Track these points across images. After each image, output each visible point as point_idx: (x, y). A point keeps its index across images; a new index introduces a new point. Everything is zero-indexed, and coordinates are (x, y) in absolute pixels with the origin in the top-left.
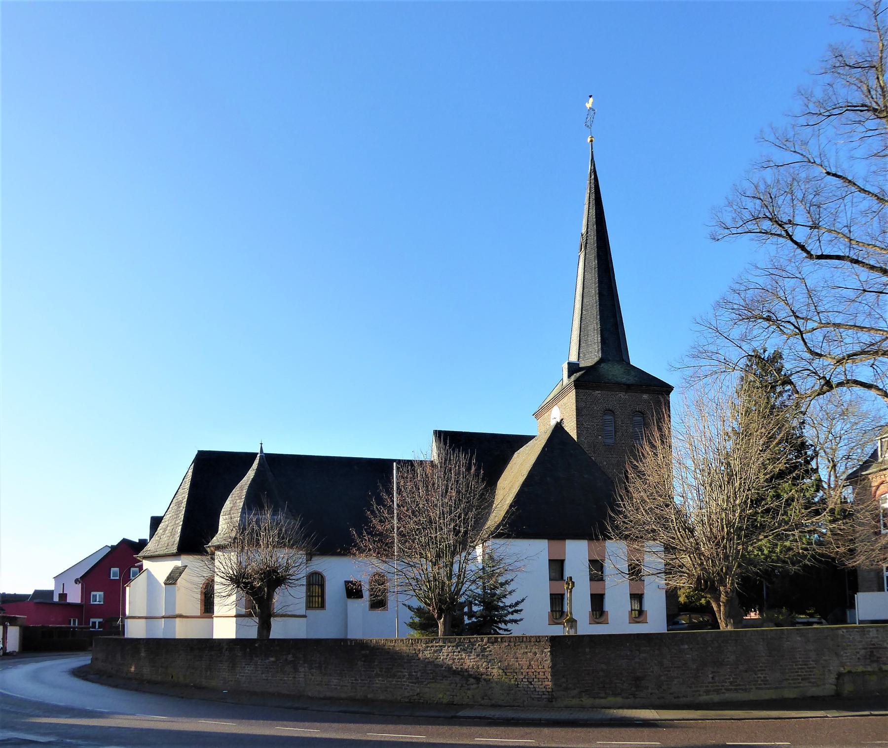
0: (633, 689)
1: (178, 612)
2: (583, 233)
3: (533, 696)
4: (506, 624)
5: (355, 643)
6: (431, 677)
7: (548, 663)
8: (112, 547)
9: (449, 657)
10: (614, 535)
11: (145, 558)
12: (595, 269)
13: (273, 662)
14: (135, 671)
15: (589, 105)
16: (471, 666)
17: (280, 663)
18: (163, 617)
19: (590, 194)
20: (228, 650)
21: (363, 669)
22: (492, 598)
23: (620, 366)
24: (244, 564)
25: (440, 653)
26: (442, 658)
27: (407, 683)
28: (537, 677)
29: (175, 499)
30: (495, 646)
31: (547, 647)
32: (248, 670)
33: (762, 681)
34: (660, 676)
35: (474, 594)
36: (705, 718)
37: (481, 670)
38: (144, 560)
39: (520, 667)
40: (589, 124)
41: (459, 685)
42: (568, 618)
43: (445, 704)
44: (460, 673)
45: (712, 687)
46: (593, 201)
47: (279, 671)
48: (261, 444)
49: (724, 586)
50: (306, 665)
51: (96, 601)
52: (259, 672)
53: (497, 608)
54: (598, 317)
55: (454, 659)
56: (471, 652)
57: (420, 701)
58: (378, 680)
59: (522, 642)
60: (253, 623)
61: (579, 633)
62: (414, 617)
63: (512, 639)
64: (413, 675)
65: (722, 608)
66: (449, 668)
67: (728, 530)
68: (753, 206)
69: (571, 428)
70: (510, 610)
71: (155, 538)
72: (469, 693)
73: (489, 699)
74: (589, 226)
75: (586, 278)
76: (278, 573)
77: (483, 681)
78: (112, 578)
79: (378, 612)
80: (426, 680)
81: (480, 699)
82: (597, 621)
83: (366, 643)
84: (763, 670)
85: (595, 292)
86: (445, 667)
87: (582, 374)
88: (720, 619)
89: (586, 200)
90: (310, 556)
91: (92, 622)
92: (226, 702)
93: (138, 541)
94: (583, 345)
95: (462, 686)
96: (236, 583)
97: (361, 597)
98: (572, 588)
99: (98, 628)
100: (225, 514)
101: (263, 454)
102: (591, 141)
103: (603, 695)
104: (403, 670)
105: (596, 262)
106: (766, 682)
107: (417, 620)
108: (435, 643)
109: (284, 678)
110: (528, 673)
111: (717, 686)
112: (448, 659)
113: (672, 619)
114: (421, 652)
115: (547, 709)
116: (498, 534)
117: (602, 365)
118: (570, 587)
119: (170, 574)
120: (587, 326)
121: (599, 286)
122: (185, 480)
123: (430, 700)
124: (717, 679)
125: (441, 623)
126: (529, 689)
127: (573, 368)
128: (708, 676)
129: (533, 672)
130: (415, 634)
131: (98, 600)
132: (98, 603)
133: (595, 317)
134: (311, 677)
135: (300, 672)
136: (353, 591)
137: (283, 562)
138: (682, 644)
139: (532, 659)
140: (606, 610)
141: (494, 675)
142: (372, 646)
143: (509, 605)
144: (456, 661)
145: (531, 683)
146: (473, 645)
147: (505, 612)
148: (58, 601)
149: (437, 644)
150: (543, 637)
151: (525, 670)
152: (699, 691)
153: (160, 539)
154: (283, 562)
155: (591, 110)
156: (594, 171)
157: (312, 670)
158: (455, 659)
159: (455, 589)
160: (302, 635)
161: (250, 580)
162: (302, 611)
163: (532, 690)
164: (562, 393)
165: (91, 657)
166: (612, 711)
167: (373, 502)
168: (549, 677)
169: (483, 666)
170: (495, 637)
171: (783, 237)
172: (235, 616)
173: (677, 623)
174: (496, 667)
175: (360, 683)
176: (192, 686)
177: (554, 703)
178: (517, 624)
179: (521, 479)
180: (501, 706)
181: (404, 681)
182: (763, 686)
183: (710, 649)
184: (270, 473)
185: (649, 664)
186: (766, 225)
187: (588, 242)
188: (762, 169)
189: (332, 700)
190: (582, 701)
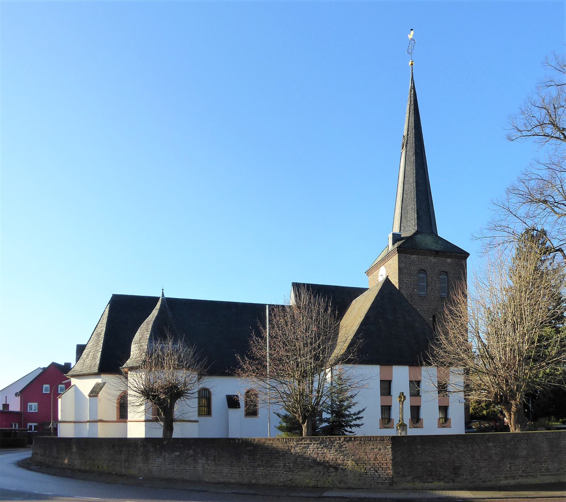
0: (453, 476)
2: (405, 135)
3: (377, 481)
4: (351, 428)
5: (241, 441)
7: (390, 456)
8: (44, 369)
10: (433, 362)
11: (73, 376)
12: (413, 163)
13: (178, 456)
14: (68, 463)
15: (410, 36)
16: (331, 459)
17: (184, 456)
18: (88, 422)
19: (410, 106)
20: (142, 446)
21: (248, 461)
22: (341, 409)
23: (431, 237)
24: (152, 381)
25: (308, 449)
26: (309, 452)
28: (381, 466)
29: (95, 331)
31: (389, 444)
32: (158, 462)
33: (545, 469)
34: (472, 466)
35: (328, 405)
36: (509, 497)
37: (339, 461)
38: (72, 378)
39: (368, 460)
40: (410, 51)
41: (322, 473)
42: (400, 423)
43: (312, 487)
44: (323, 464)
45: (509, 474)
46: (412, 110)
47: (183, 462)
48: (163, 290)
49: (514, 400)
50: (204, 458)
51: (32, 410)
52: (167, 463)
53: (344, 416)
54: (415, 199)
56: (331, 448)
57: (292, 485)
58: (260, 470)
59: (370, 440)
60: (159, 426)
61: (408, 434)
62: (281, 422)
63: (362, 439)
65: (512, 416)
66: (315, 460)
67: (519, 359)
68: (540, 115)
69: (395, 281)
70: (354, 417)
71: (81, 361)
73: (345, 483)
74: (409, 130)
75: (406, 169)
76: (179, 389)
77: (340, 470)
78: (44, 392)
79: (251, 419)
80: (297, 469)
82: (385, 426)
83: (250, 441)
84: (546, 462)
85: (413, 180)
86: (311, 460)
87: (403, 243)
88: (511, 424)
89: (407, 110)
90: (201, 375)
91: (29, 426)
92: (143, 486)
93: (64, 364)
94: (403, 220)
95: (324, 474)
96: (147, 396)
97: (239, 407)
98: (403, 401)
99: (34, 430)
101: (164, 298)
102: (412, 64)
103: (430, 480)
105: (414, 157)
106: (548, 471)
107: (284, 424)
108: (304, 441)
109: (186, 467)
110: (374, 464)
111: (513, 473)
112: (313, 454)
113: (468, 426)
114: (293, 448)
115: (390, 491)
116: (345, 359)
117: (418, 236)
118: (402, 400)
119: (93, 389)
122: (103, 317)
123: (300, 484)
124: (513, 468)
125: (304, 427)
126: (375, 476)
127: (396, 238)
128: (506, 466)
129: (378, 463)
130: (283, 435)
131: (33, 409)
132: (34, 411)
133: (413, 199)
134: (208, 467)
135: (199, 463)
136: (232, 402)
137: (182, 380)
138: (489, 443)
139: (378, 453)
140: (450, 418)
142: (255, 443)
143: (353, 413)
144: (320, 455)
145: (376, 471)
146: (333, 443)
147: (351, 418)
148: (2, 409)
149: (306, 442)
150: (386, 437)
151: (372, 462)
152: (500, 477)
153: (85, 362)
154: (182, 380)
155: (412, 41)
156: (413, 88)
157: (209, 462)
158: (319, 453)
159: (315, 401)
160: (196, 436)
161: (157, 394)
162: (196, 418)
163: (378, 476)
165: (32, 452)
166: (434, 492)
167: (253, 334)
168: (391, 467)
170: (349, 437)
171: (561, 139)
172: (145, 421)
173: (471, 428)
174: (350, 459)
175: (246, 471)
176: (114, 474)
177: (394, 486)
178: (359, 427)
179: (360, 320)
180: (354, 489)
181: (280, 470)
182: (546, 473)
183: (508, 446)
184: (170, 312)
185: (464, 457)
186: (549, 130)
187: (408, 142)
188: (545, 87)
189: (226, 484)
190: (414, 484)
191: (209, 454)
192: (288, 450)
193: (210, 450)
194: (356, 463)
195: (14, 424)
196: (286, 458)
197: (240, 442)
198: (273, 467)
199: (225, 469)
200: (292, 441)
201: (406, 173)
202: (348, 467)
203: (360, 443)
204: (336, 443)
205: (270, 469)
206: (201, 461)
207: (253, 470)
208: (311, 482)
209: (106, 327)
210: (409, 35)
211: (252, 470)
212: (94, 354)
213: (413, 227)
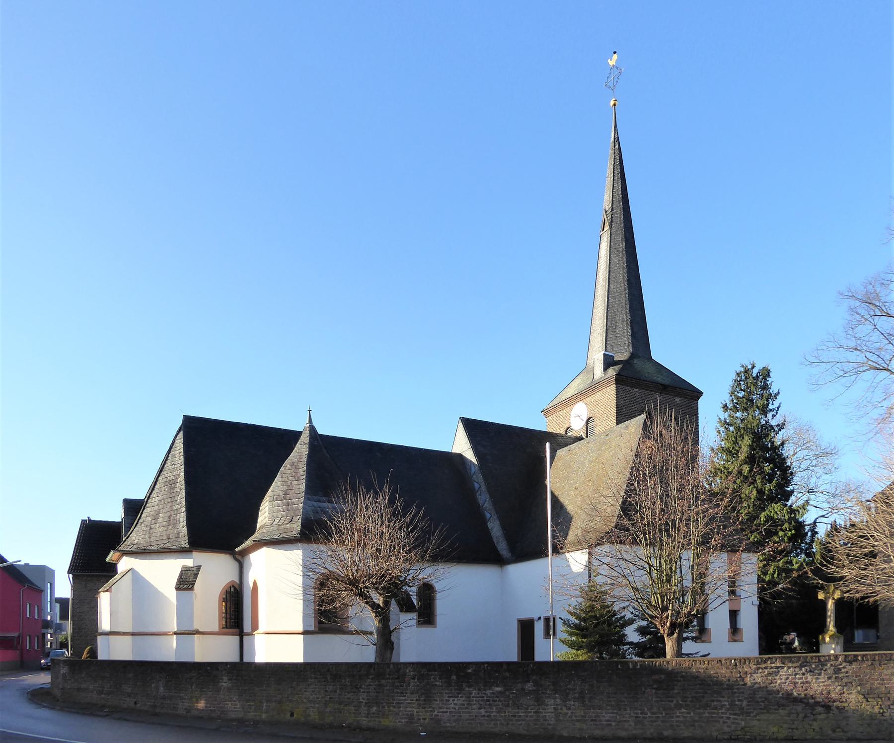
1: (196, 626)
2: (607, 209)
5: (640, 665)
6: (762, 707)
9: (788, 681)
13: (500, 692)
15: (612, 63)
19: (614, 166)
21: (654, 699)
26: (779, 682)
27: (728, 715)
30: (854, 666)
41: (801, 715)
48: (310, 411)
54: (628, 307)
55: (795, 683)
56: (820, 674)
57: (746, 737)
58: (680, 713)
64: (736, 705)
66: (788, 696)
72: (815, 725)
73: (843, 731)
74: (615, 202)
77: (835, 709)
80: (756, 711)
81: (830, 732)
85: (624, 278)
95: (805, 717)
100: (276, 498)
102: (615, 105)
104: (721, 699)
108: (771, 663)
117: (635, 361)
120: (615, 315)
121: (628, 273)
123: (760, 735)
133: (624, 306)
135: (547, 705)
141: (851, 702)
142: (670, 669)
144: (798, 685)
146: (823, 665)
149: (773, 665)
155: (615, 69)
156: (617, 140)
158: (797, 683)
164: (594, 387)
169: (835, 690)
172: (305, 633)
174: (854, 692)
181: (722, 713)
191: (570, 689)
192: (738, 679)
193: (573, 682)
194: (865, 697)
195: (664, 655)
196: (735, 693)
197: (639, 667)
198: (708, 708)
199: (604, 714)
200: (747, 663)
201: (611, 266)
202: (850, 705)
203: (872, 664)
204: (829, 665)
205: (701, 711)
206: (552, 701)
207: (666, 714)
208: (780, 731)
209: (184, 470)
210: (609, 60)
211: (664, 715)
212: (169, 517)
213: (626, 347)
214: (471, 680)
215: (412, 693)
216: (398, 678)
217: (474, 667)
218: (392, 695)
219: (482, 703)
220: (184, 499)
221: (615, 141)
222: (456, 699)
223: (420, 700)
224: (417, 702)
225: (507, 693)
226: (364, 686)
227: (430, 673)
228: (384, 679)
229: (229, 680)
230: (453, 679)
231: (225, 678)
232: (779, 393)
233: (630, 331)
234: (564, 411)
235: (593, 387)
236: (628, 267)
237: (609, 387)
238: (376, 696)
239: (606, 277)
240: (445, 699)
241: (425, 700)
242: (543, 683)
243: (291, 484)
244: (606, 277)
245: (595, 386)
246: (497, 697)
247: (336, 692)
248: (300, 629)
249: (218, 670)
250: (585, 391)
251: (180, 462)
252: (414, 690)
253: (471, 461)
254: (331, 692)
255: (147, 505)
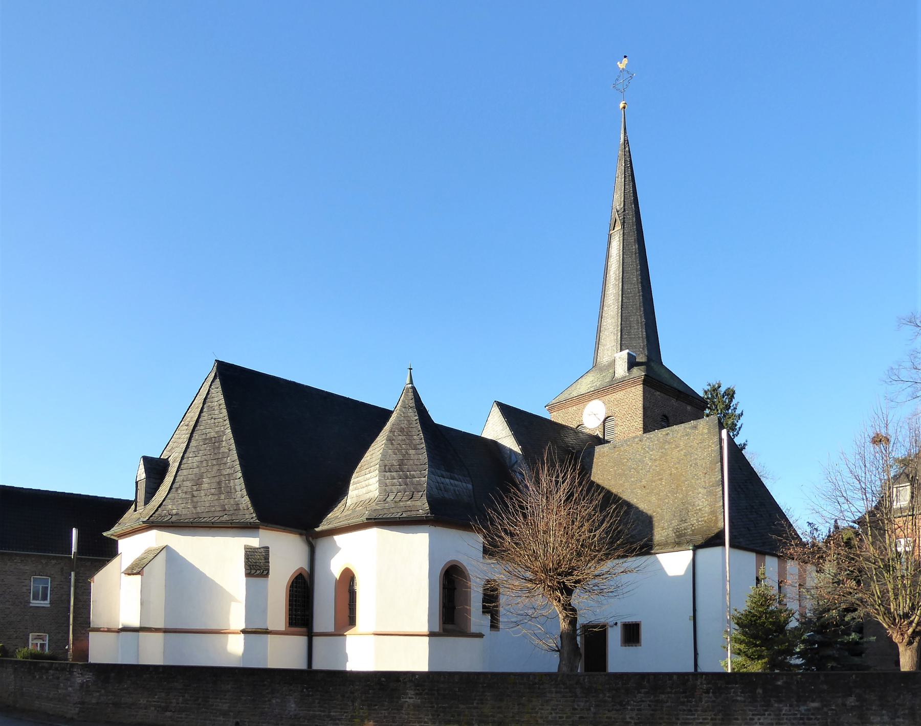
2: (618, 209)
13: (817, 709)
40: (620, 87)
48: (411, 369)
50: (884, 712)
54: (642, 309)
74: (626, 203)
85: (637, 280)
100: (389, 469)
102: (624, 108)
156: (626, 142)
157: (897, 720)
164: (614, 385)
172: (244, 632)
193: (902, 697)
212: (219, 483)
213: (641, 349)
214: (780, 695)
215: (704, 711)
216: (684, 692)
217: (785, 679)
218: (675, 713)
219: (794, 722)
220: (238, 462)
221: (625, 143)
222: (762, 717)
223: (715, 719)
224: (712, 721)
225: (825, 709)
226: (632, 702)
227: (730, 686)
228: (663, 693)
229: (417, 694)
230: (759, 693)
231: (411, 693)
232: (742, 414)
233: (645, 333)
234: (574, 408)
235: (615, 385)
236: (641, 270)
237: (634, 387)
238: (652, 715)
239: (619, 276)
240: (748, 718)
241: (723, 719)
242: (867, 696)
243: (407, 453)
244: (619, 276)
245: (617, 384)
246: (813, 714)
247: (590, 709)
248: (425, 629)
249: (400, 681)
250: (605, 388)
251: (221, 416)
252: (708, 707)
253: (511, 450)
254: (582, 710)
255: (182, 466)
